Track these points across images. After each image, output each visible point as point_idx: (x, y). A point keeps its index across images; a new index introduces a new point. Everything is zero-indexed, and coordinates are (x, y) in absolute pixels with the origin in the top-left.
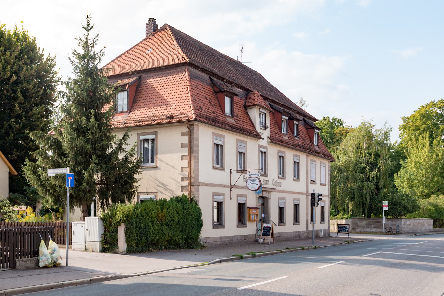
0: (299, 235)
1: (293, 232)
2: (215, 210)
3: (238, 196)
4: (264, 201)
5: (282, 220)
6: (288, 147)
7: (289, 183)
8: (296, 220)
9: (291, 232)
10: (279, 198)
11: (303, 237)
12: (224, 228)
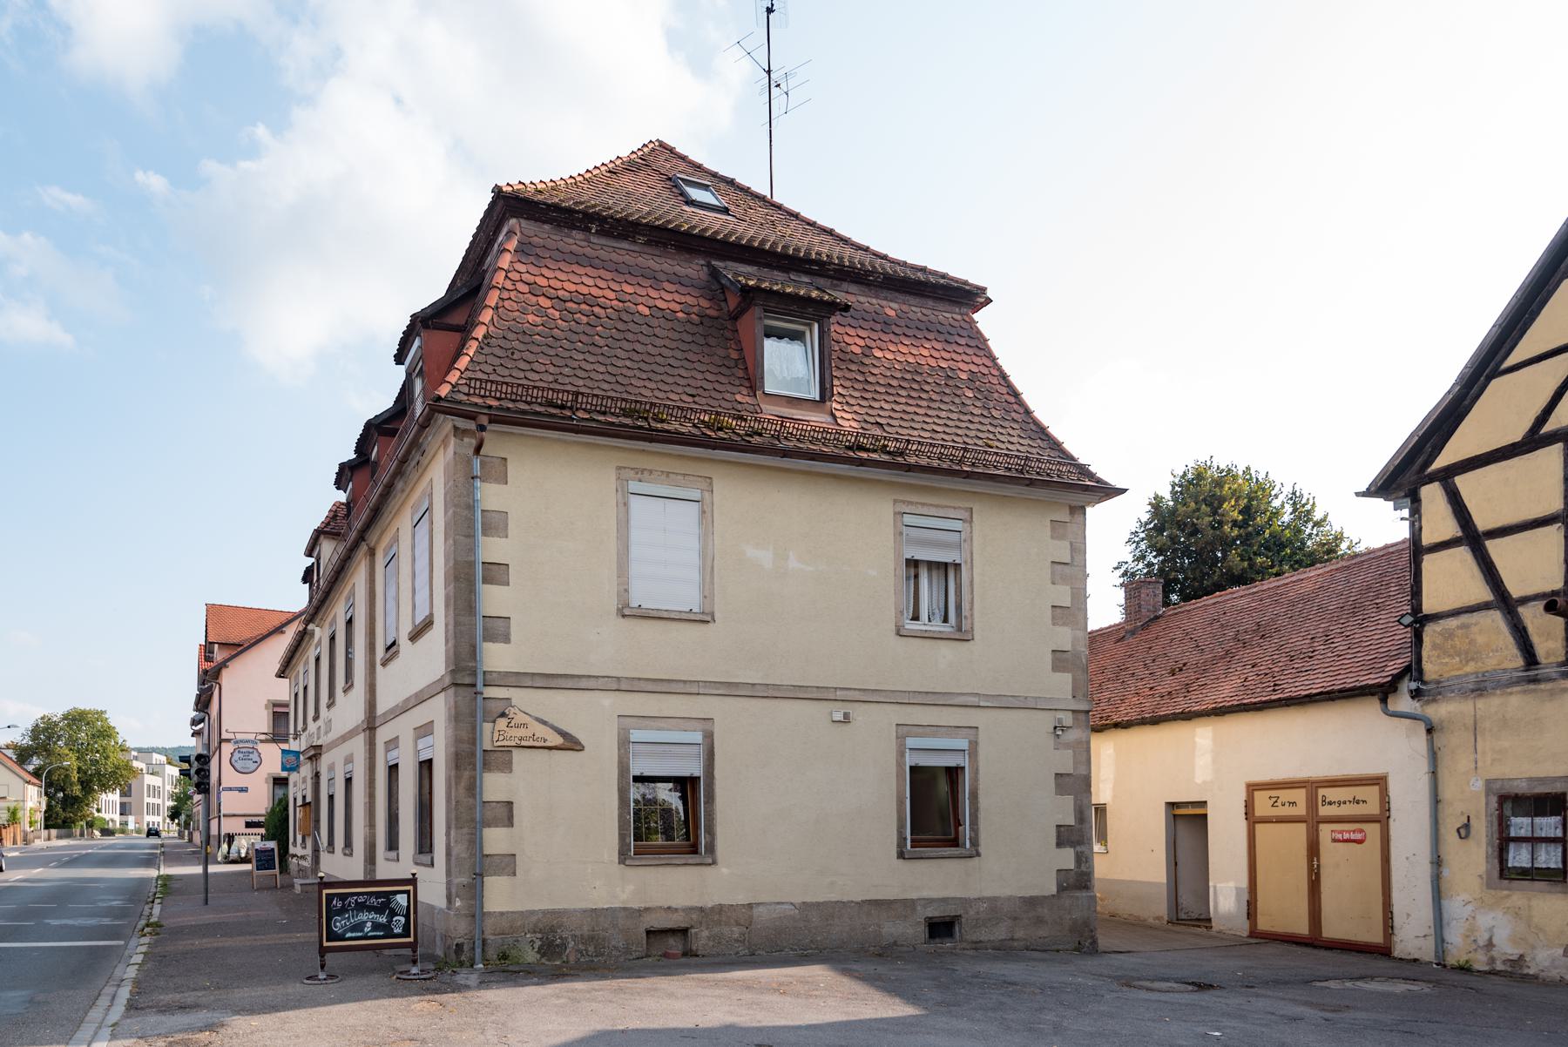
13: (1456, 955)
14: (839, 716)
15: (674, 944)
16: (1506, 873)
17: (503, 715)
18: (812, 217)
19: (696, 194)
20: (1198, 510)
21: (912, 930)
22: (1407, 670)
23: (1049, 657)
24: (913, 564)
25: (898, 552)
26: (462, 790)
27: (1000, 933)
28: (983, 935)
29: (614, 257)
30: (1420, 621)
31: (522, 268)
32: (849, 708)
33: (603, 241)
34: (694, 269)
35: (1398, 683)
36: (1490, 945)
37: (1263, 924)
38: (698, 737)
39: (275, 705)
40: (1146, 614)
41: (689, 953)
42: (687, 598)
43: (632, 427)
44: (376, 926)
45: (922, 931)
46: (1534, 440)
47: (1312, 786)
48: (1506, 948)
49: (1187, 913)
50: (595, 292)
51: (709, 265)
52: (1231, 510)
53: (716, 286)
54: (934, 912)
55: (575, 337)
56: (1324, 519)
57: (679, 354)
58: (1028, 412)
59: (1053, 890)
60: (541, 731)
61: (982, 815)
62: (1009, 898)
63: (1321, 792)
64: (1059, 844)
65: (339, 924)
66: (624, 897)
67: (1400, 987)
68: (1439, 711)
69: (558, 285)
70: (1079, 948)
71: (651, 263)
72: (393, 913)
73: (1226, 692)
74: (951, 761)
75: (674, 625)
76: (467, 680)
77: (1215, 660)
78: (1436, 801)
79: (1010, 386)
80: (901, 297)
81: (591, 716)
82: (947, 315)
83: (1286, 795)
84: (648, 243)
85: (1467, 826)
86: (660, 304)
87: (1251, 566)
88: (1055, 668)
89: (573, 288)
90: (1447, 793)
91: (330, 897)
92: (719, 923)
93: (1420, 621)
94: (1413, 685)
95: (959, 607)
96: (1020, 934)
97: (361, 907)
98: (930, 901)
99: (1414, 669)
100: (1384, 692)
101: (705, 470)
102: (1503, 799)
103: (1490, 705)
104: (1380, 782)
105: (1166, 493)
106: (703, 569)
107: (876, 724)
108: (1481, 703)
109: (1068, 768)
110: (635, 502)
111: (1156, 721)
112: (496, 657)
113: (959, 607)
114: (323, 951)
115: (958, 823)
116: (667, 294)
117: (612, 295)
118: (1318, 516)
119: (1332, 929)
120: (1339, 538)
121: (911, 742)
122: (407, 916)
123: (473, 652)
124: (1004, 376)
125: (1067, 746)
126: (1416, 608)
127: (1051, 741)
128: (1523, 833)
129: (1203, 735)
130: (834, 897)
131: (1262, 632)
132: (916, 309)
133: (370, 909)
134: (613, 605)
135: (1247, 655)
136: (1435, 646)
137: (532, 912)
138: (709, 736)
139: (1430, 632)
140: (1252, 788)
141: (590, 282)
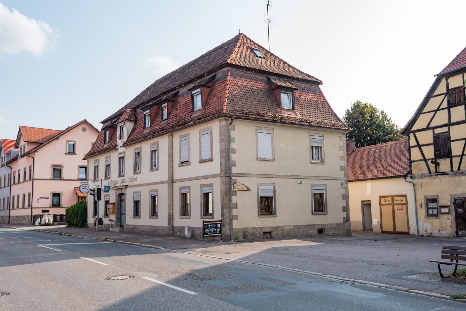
0: (156, 230)
1: (150, 226)
2: (188, 202)
3: (181, 188)
4: (121, 198)
5: (137, 213)
6: (141, 141)
7: (147, 175)
8: (154, 212)
9: (147, 226)
10: (134, 193)
11: (163, 233)
12: (157, 218)
13: (421, 233)
14: (299, 182)
15: (268, 235)
16: (429, 215)
17: (235, 183)
18: (282, 58)
19: (258, 53)
20: (359, 116)
21: (315, 232)
22: (409, 172)
23: (339, 168)
24: (312, 146)
25: (310, 145)
26: (227, 200)
27: (332, 232)
28: (329, 232)
29: (249, 75)
30: (411, 162)
31: (232, 79)
32: (302, 180)
33: (246, 72)
34: (264, 78)
35: (407, 175)
36: (427, 230)
37: (384, 229)
38: (272, 187)
39: (54, 166)
40: (352, 150)
41: (271, 237)
42: (269, 156)
43: (260, 119)
44: (214, 231)
45: (317, 232)
46: (428, 128)
47: (393, 197)
48: (429, 231)
49: (367, 228)
50: (246, 84)
51: (267, 77)
52: (367, 117)
53: (269, 82)
54: (319, 227)
55: (244, 96)
56: (390, 120)
57: (264, 99)
58: (332, 111)
59: (342, 222)
60: (243, 187)
61: (328, 205)
62: (334, 224)
63: (394, 198)
64: (343, 211)
65: (207, 231)
66: (259, 224)
67: (411, 239)
68: (415, 181)
69: (239, 83)
70: (348, 235)
71: (256, 77)
72: (217, 228)
73: (373, 174)
74: (321, 192)
75: (267, 162)
76: (228, 175)
77: (370, 165)
78: (416, 200)
79: (328, 104)
80: (305, 83)
81: (252, 183)
82: (314, 87)
83: (387, 199)
84: (255, 72)
85: (421, 205)
86: (259, 87)
87: (373, 132)
88: (341, 170)
89: (242, 84)
90: (417, 199)
91: (205, 225)
92: (277, 230)
93: (411, 162)
94: (410, 175)
95: (321, 157)
96: (336, 232)
97: (211, 227)
98: (318, 225)
99: (410, 172)
100: (405, 176)
101: (273, 127)
102: (427, 200)
103: (424, 180)
104: (405, 196)
105: (350, 109)
106: (272, 149)
107: (307, 183)
108: (422, 180)
109: (344, 194)
110: (259, 134)
111: (358, 180)
112: (234, 170)
113: (321, 157)
114: (204, 237)
115: (323, 207)
116: (259, 85)
117: (249, 85)
118: (388, 118)
119: (398, 230)
120: (393, 125)
121: (314, 188)
122: (220, 229)
123: (230, 169)
124: (327, 102)
125: (344, 188)
126: (410, 159)
127: (340, 187)
128: (431, 207)
129: (369, 184)
130: (300, 224)
131: (380, 158)
132: (308, 86)
133: (213, 227)
134: (255, 158)
135: (377, 165)
136: (414, 168)
137: (242, 228)
138: (274, 187)
139: (413, 164)
140: (380, 197)
141: (245, 82)
